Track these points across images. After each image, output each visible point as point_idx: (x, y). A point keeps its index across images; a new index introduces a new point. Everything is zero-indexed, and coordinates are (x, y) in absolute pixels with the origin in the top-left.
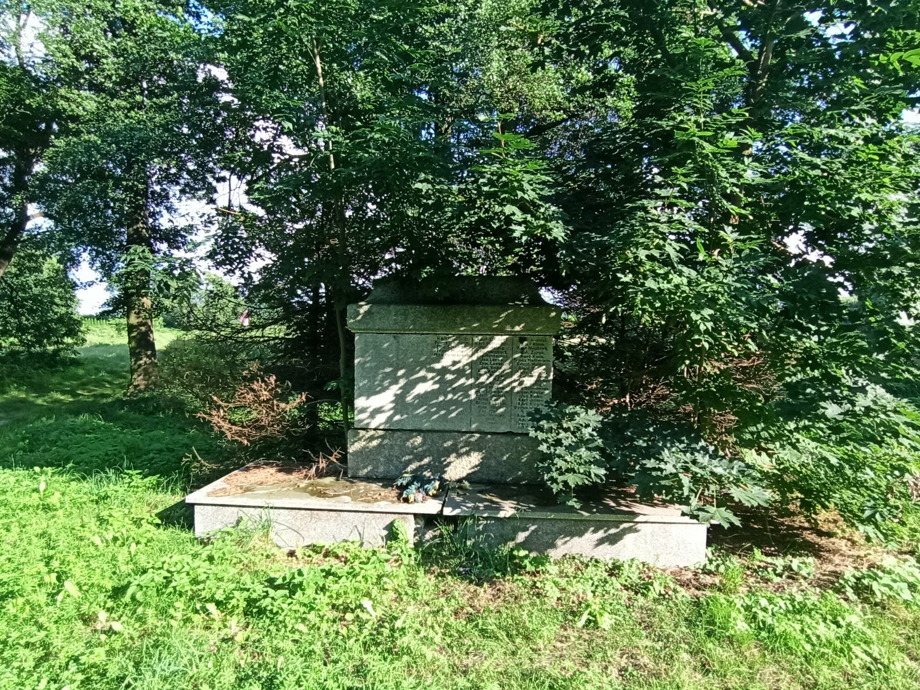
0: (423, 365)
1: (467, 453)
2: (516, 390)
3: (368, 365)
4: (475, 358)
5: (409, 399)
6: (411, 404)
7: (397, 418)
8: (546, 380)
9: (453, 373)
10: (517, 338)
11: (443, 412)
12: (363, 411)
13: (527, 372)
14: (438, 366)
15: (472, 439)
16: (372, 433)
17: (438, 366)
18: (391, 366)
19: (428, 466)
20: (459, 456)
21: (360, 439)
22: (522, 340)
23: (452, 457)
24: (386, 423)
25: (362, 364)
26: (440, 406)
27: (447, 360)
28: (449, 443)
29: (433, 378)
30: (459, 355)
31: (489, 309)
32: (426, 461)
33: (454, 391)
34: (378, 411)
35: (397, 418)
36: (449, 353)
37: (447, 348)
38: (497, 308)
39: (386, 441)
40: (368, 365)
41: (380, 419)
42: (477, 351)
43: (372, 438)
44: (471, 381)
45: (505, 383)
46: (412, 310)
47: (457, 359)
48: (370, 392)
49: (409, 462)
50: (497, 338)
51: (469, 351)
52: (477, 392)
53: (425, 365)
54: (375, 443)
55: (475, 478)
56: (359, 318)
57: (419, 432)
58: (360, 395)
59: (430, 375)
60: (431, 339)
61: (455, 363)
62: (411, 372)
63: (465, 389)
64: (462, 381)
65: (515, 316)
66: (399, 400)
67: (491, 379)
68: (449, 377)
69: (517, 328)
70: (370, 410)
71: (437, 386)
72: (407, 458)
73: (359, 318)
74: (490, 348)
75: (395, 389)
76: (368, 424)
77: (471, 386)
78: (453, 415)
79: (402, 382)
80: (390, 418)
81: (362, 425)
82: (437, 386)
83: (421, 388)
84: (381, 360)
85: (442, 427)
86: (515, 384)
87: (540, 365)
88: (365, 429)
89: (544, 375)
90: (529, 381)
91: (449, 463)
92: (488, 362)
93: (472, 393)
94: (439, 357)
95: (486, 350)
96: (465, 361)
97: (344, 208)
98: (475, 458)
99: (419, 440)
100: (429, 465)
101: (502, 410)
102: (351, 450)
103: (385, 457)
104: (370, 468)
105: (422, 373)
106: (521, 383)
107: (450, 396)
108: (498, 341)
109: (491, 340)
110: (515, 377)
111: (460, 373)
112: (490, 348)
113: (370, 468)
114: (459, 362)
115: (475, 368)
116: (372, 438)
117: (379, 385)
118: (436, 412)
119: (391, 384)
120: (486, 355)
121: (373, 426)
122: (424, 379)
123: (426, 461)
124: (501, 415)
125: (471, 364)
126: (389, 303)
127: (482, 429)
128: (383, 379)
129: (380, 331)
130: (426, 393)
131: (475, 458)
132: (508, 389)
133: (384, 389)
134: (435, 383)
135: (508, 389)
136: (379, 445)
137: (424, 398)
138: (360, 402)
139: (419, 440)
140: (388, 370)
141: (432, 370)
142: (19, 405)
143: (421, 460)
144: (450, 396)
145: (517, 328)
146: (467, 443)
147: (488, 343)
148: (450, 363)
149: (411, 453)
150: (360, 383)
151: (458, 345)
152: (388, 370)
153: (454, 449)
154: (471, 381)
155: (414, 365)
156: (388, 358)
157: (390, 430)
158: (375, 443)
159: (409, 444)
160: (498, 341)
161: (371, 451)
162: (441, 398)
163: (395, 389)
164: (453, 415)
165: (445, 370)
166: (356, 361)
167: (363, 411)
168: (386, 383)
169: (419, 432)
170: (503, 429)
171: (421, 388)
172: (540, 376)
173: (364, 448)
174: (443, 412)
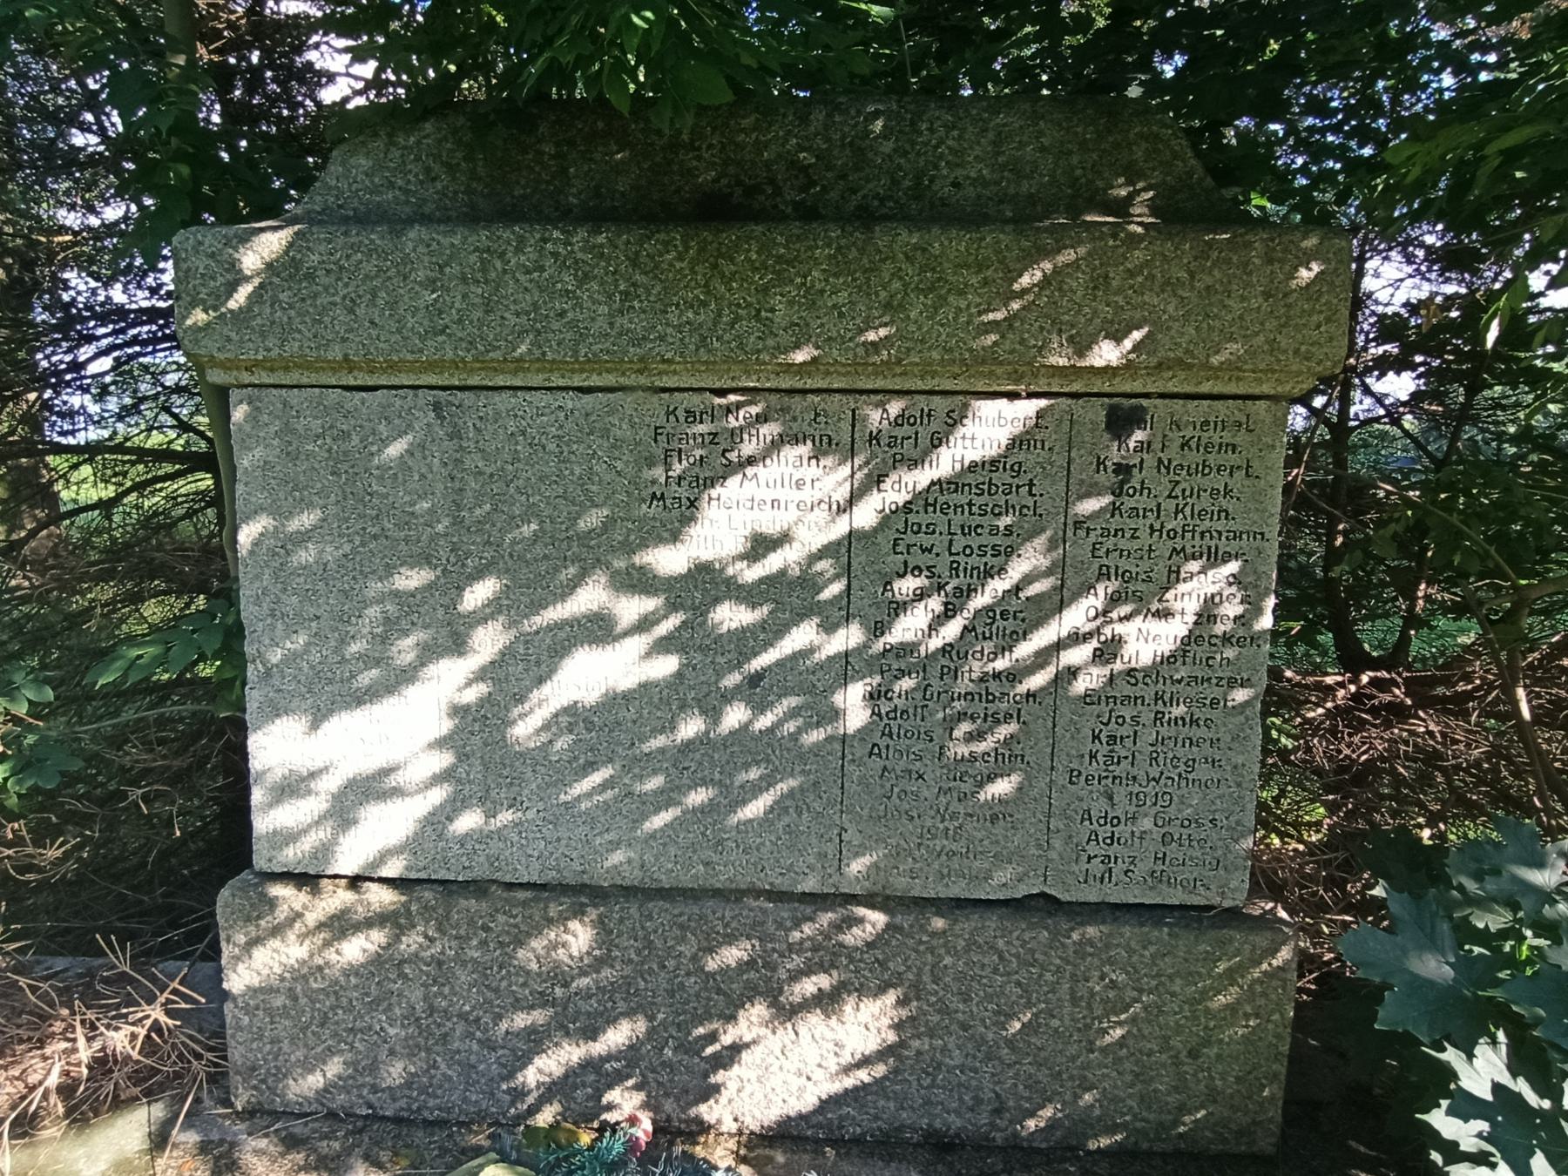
0: (588, 556)
1: (827, 1002)
2: (1081, 685)
3: (306, 556)
4: (866, 515)
5: (525, 728)
6: (538, 757)
7: (468, 821)
8: (1244, 631)
9: (748, 595)
10: (1097, 412)
11: (698, 797)
12: (292, 787)
13: (1143, 593)
14: (669, 560)
15: (854, 937)
16: (336, 898)
17: (669, 560)
18: (425, 560)
19: (627, 1064)
20: (787, 1013)
21: (277, 931)
22: (1121, 421)
23: (751, 1021)
24: (411, 846)
25: (281, 545)
26: (687, 763)
27: (718, 530)
28: (732, 955)
29: (644, 624)
30: (782, 502)
31: (951, 244)
32: (617, 1036)
33: (757, 690)
34: (371, 788)
35: (468, 821)
36: (732, 488)
37: (723, 462)
38: (996, 239)
39: (412, 942)
40: (306, 556)
41: (381, 833)
42: (876, 480)
43: (340, 926)
44: (850, 637)
45: (1025, 650)
46: (525, 252)
47: (770, 524)
48: (330, 693)
49: (536, 1041)
50: (987, 409)
51: (835, 479)
52: (872, 697)
53: (613, 553)
54: (355, 949)
55: (859, 1123)
56: (242, 295)
57: (580, 895)
58: (275, 711)
59: (630, 608)
60: (635, 414)
61: (761, 545)
62: (531, 585)
63: (813, 683)
64: (802, 636)
65: (1100, 282)
66: (476, 735)
67: (951, 630)
68: (731, 616)
69: (1107, 354)
70: (329, 784)
71: (667, 665)
72: (521, 1020)
73: (242, 295)
74: (945, 463)
75: (450, 682)
76: (325, 851)
77: (845, 667)
78: (755, 809)
79: (488, 642)
80: (436, 821)
81: (292, 856)
82: (667, 665)
83: (587, 676)
84: (377, 534)
85: (693, 875)
86: (1077, 655)
87: (1215, 559)
88: (307, 880)
89: (1232, 609)
90: (1148, 640)
91: (736, 1049)
92: (946, 536)
93: (854, 705)
94: (678, 516)
95: (922, 478)
96: (817, 532)
97: (280, 113)
98: (866, 1025)
99: (579, 938)
100: (630, 1055)
101: (1002, 787)
102: (238, 980)
103: (410, 1017)
104: (334, 1068)
105: (590, 597)
106: (1108, 651)
107: (735, 716)
108: (991, 426)
109: (955, 420)
110: (1076, 616)
111: (789, 597)
112: (945, 463)
113: (334, 1068)
114: (782, 540)
115: (864, 571)
116: (340, 926)
117: (368, 660)
118: (664, 799)
119: (429, 654)
120: (924, 500)
121: (348, 860)
122: (599, 630)
123: (617, 1036)
124: (999, 812)
125: (845, 550)
126: (397, 223)
127: (900, 884)
128: (391, 629)
129: (361, 377)
130: (615, 701)
131: (866, 1025)
132: (1038, 680)
133: (399, 679)
134: (663, 646)
135: (1038, 680)
136: (377, 961)
137: (604, 727)
138: (274, 747)
139: (579, 938)
140: (412, 579)
141: (639, 581)
142: (1078, 909)
143: (592, 1034)
144: (735, 716)
145: (1107, 354)
146: (824, 956)
147: (937, 441)
148: (734, 543)
149: (543, 1000)
150: (274, 649)
151: (776, 445)
152: (412, 579)
153: (763, 984)
154: (850, 637)
155: (550, 549)
156: (408, 519)
157: (435, 887)
158: (355, 949)
159: (529, 955)
160: (991, 426)
161: (335, 989)
162: (691, 727)
163: (450, 682)
164: (755, 809)
165: (706, 583)
166: (247, 535)
167: (292, 787)
168: (405, 649)
169: (580, 895)
170: (1003, 881)
171: (587, 676)
172: (1207, 615)
173: (302, 974)
174: (698, 797)
